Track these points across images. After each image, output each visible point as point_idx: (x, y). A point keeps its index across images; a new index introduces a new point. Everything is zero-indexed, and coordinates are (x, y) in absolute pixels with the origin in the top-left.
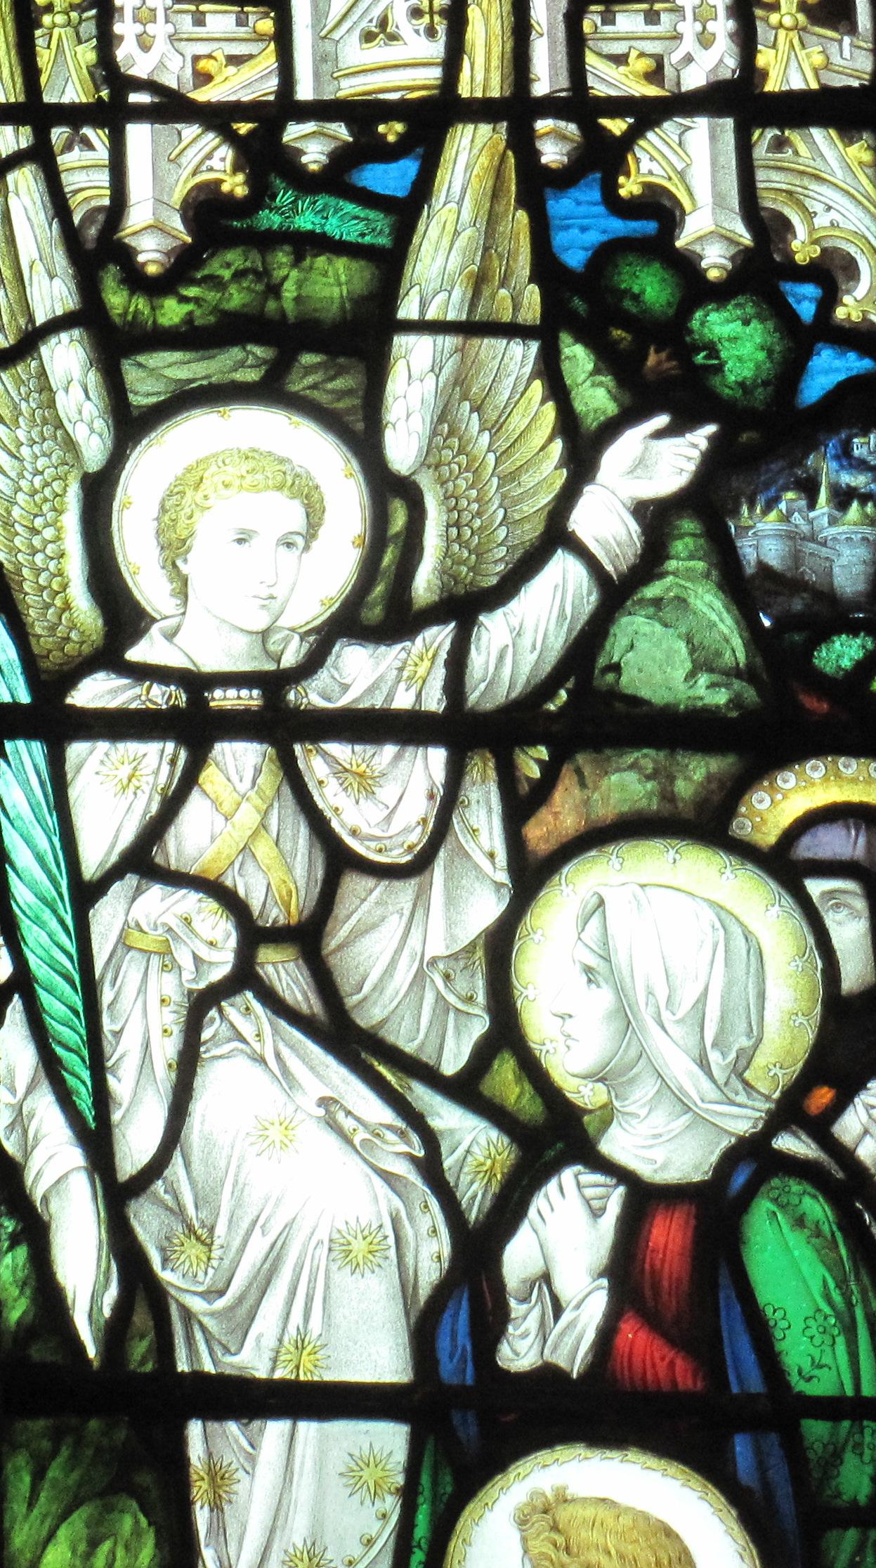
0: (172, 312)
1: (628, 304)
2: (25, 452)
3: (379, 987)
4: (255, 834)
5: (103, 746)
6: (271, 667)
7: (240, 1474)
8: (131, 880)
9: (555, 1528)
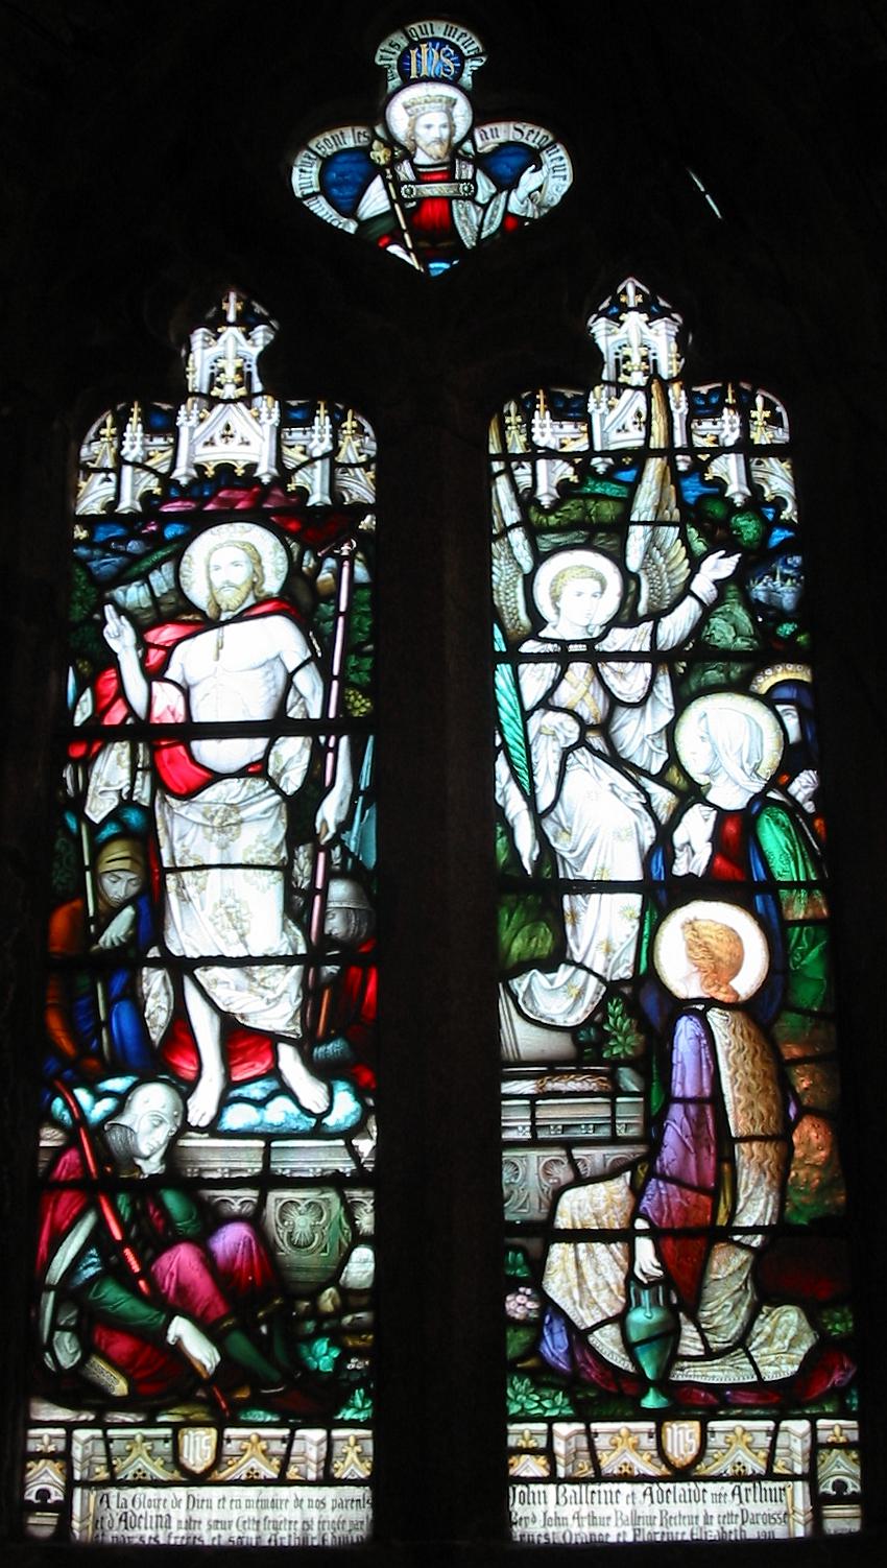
0: (553, 520)
1: (709, 514)
2: (503, 568)
3: (629, 744)
4: (584, 695)
5: (532, 665)
6: (589, 637)
7: (582, 914)
8: (542, 711)
9: (693, 929)
